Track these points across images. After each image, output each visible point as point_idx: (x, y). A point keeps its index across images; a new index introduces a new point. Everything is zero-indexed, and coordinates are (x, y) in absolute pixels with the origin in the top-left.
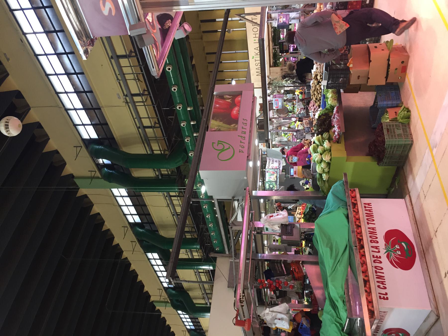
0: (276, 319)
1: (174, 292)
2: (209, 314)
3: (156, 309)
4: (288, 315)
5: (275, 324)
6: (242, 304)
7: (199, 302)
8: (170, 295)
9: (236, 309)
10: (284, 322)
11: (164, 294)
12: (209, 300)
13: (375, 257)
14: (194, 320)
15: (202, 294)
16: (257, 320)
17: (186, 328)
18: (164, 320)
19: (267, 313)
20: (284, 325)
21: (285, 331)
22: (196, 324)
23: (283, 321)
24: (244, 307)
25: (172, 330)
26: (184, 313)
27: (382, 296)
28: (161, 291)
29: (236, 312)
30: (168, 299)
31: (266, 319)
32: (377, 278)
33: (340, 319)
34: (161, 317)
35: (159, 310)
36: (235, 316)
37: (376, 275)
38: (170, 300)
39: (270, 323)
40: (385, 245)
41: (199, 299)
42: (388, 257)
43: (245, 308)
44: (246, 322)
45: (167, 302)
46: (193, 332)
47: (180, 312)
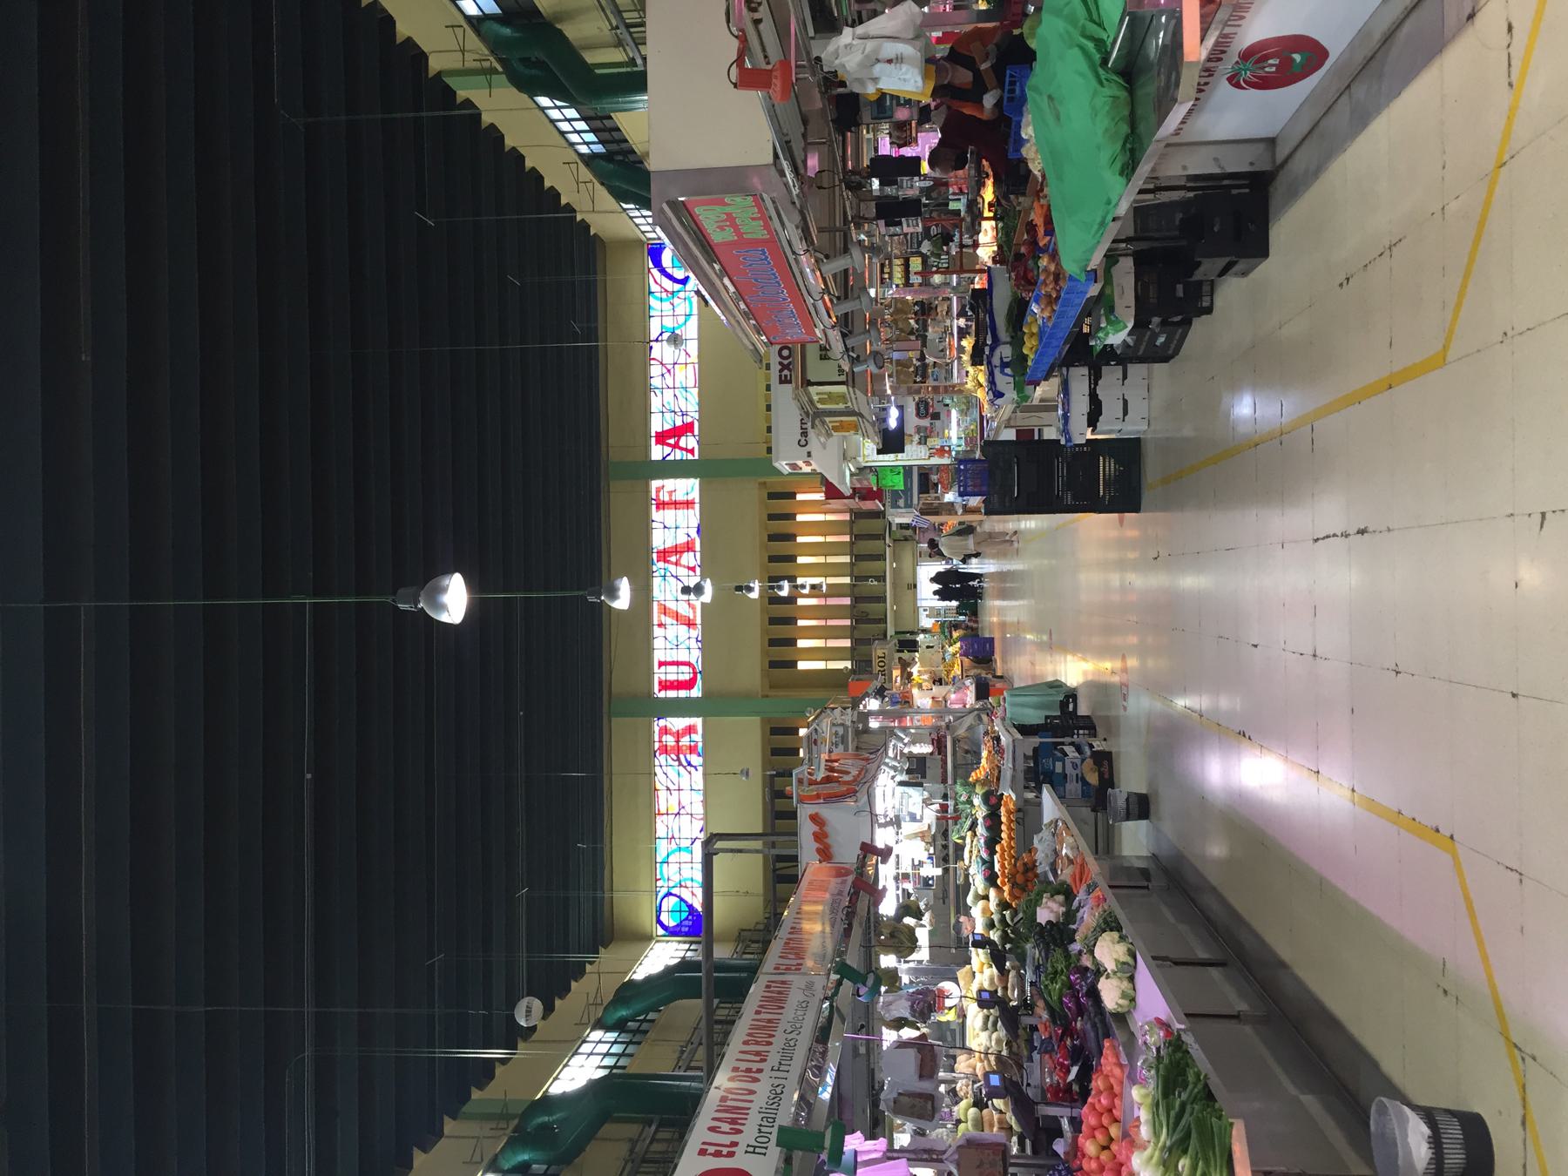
0: (878, 61)
1: (507, 31)
2: (646, 98)
3: (459, 100)
4: (918, 43)
5: (875, 80)
6: (757, 16)
7: (604, 57)
8: (495, 45)
9: (734, 29)
10: (904, 67)
11: (473, 41)
12: (640, 47)
14: (599, 122)
15: (613, 29)
16: (813, 74)
17: (576, 151)
18: (495, 135)
19: (846, 46)
20: (905, 80)
21: (908, 102)
22: (606, 136)
23: (903, 65)
24: (761, 27)
25: (529, 164)
26: (559, 103)
28: (459, 31)
29: (735, 43)
30: (491, 58)
31: (844, 66)
33: (1100, 25)
34: (506, 150)
35: (468, 103)
36: (735, 58)
38: (500, 60)
39: (858, 80)
41: (603, 50)
43: (767, 27)
44: (774, 73)
45: (493, 71)
46: (603, 163)
47: (544, 101)
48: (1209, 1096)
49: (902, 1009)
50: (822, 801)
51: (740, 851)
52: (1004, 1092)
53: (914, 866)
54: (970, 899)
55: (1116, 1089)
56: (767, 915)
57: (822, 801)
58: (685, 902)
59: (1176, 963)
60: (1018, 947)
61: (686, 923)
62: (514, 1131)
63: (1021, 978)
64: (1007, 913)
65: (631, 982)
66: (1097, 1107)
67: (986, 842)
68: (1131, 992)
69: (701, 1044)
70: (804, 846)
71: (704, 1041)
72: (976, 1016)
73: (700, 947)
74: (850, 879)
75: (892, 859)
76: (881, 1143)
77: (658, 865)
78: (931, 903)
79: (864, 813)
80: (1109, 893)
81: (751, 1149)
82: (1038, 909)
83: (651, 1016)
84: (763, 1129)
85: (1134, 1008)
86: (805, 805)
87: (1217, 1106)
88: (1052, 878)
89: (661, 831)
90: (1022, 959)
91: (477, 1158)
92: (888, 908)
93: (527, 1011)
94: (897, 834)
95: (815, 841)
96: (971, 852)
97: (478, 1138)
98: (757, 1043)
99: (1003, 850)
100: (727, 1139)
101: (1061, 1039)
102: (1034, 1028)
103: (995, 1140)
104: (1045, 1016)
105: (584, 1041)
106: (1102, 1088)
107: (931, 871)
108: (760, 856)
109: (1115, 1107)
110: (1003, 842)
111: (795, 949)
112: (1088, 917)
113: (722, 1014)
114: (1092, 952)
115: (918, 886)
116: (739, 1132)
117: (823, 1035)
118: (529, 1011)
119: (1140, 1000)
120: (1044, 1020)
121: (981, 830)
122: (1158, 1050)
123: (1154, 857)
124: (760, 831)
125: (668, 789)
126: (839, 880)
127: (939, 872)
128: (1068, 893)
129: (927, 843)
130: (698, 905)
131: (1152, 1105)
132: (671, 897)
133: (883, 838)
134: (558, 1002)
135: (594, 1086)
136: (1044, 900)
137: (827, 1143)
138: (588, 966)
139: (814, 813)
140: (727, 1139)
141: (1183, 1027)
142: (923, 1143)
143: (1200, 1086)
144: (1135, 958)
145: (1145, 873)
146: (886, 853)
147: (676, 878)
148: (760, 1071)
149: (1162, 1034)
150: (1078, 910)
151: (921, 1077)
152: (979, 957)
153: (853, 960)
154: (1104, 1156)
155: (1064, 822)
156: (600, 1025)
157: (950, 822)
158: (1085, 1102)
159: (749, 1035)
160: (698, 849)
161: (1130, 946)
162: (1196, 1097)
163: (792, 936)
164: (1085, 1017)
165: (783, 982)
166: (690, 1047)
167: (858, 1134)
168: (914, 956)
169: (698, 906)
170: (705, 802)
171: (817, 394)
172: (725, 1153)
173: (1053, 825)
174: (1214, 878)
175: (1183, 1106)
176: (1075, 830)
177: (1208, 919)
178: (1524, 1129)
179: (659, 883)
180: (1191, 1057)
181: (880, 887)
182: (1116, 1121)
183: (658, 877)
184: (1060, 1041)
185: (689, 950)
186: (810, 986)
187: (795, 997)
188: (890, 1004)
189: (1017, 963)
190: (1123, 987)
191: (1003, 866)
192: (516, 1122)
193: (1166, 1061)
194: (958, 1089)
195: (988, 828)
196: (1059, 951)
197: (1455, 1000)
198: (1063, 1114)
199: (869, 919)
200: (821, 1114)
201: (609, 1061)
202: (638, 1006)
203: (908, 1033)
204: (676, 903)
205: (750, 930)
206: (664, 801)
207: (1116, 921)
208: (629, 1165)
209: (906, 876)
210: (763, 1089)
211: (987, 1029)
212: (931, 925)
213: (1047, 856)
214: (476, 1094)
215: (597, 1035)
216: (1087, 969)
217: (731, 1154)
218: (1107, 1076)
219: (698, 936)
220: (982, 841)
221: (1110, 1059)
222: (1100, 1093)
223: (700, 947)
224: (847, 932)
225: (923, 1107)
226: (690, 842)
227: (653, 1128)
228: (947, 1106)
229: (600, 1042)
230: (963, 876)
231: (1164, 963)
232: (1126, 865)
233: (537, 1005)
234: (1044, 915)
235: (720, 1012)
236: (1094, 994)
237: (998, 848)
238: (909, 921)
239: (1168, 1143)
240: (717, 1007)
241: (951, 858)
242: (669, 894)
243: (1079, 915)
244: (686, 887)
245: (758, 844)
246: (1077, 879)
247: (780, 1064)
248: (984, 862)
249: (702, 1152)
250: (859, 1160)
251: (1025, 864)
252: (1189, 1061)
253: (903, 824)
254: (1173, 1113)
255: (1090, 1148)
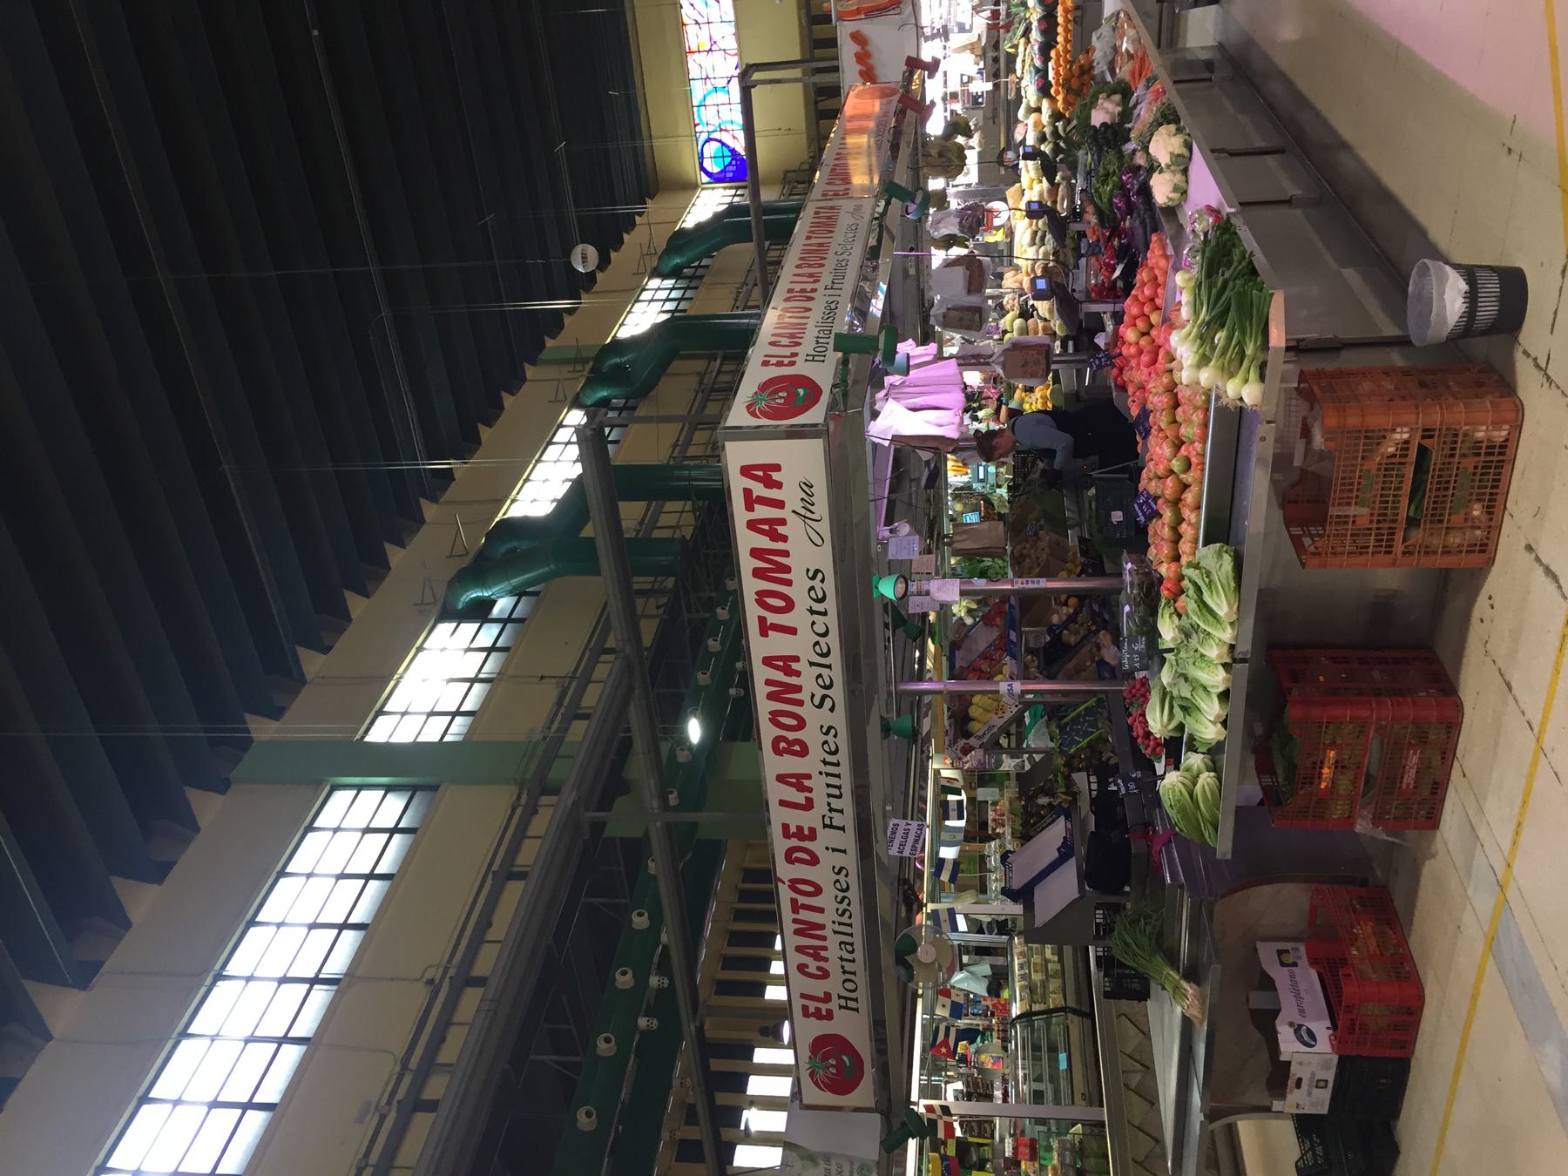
13: (794, 835)
27: (812, 1006)
32: (797, 932)
37: (795, 921)
40: (810, 1057)
42: (812, 1075)
48: (1253, 272)
49: (950, 227)
50: (863, 16)
51: (778, 81)
52: (1050, 293)
53: (963, 84)
54: (1021, 114)
55: (1160, 279)
56: (812, 154)
57: (863, 16)
58: (728, 147)
59: (1232, 155)
60: (1070, 156)
61: (731, 168)
62: (591, 371)
63: (1071, 188)
64: (1060, 124)
65: (682, 230)
66: (1140, 298)
67: (1040, 49)
68: (1184, 185)
69: (756, 285)
70: (846, 69)
71: (758, 282)
72: (1023, 233)
73: (746, 192)
74: (896, 98)
75: (939, 75)
76: (932, 348)
77: (695, 109)
78: (981, 124)
79: (910, 26)
80: (1170, 85)
81: (811, 358)
82: (1093, 112)
83: (705, 262)
84: (820, 340)
85: (1185, 200)
86: (846, 23)
87: (1259, 279)
88: (1109, 78)
89: (694, 72)
90: (1073, 167)
91: (561, 396)
92: (935, 126)
93: (583, 258)
94: (945, 48)
95: (858, 62)
96: (1024, 61)
97: (559, 380)
98: (810, 266)
99: (1058, 55)
100: (787, 351)
101: (1109, 239)
102: (1082, 235)
103: (1040, 342)
104: (1094, 220)
105: (644, 290)
106: (1146, 280)
107: (982, 86)
108: (800, 85)
109: (1157, 296)
110: (1059, 46)
111: (841, 175)
112: (1145, 112)
113: (773, 255)
114: (1146, 149)
115: (967, 105)
116: (798, 344)
117: (873, 253)
118: (584, 258)
119: (1192, 191)
120: (1092, 224)
121: (1035, 35)
122: (1206, 234)
123: (1221, 46)
124: (798, 57)
125: (697, 23)
126: (885, 100)
127: (989, 86)
128: (1125, 91)
129: (977, 56)
130: (740, 147)
131: (1194, 287)
132: (712, 142)
133: (928, 52)
134: (613, 255)
135: (658, 330)
136: (1100, 101)
137: (881, 345)
138: (637, 218)
139: (854, 31)
140: (787, 351)
141: (1233, 210)
142: (970, 350)
143: (1244, 264)
144: (1190, 149)
145: (1209, 65)
146: (933, 67)
147: (715, 121)
148: (814, 290)
149: (1211, 220)
150: (1135, 107)
151: (969, 292)
152: (1029, 170)
153: (902, 178)
154: (1143, 342)
155: (1127, 14)
156: (656, 273)
157: (1002, 31)
158: (1128, 295)
159: (801, 259)
160: (735, 87)
161: (1187, 137)
162: (1239, 274)
163: (837, 162)
164: (1135, 215)
165: (832, 208)
166: (745, 287)
167: (910, 341)
168: (960, 179)
169: (740, 149)
170: (738, 35)
171: (792, 631)
172: (786, 363)
173: (1114, 19)
174: (1283, 61)
175: (1225, 284)
176: (1137, 21)
177: (1272, 108)
178: (1563, 277)
179: (698, 129)
180: (1239, 238)
181: (928, 102)
182: (1158, 308)
183: (697, 122)
184: (1108, 242)
185: (735, 195)
186: (858, 208)
187: (845, 220)
188: (939, 222)
189: (1069, 173)
190: (1175, 181)
191: (1057, 73)
192: (591, 364)
193: (1213, 243)
194: (1004, 303)
195: (1043, 32)
196: (1112, 152)
197: (1518, 158)
198: (1105, 309)
199: (916, 140)
200: (873, 328)
201: (670, 306)
202: (690, 254)
203: (956, 251)
204: (718, 149)
205: (794, 171)
206: (694, 37)
207: (1175, 113)
208: (700, 394)
209: (954, 96)
210: (818, 308)
211: (1035, 244)
212: (980, 146)
213: (1105, 54)
214: (550, 343)
215: (655, 283)
216: (1140, 167)
217: (792, 364)
218: (1152, 268)
219: (744, 180)
220: (1036, 47)
221: (1156, 252)
222: (1144, 284)
223: (746, 192)
224: (895, 148)
225: (970, 318)
226: (726, 81)
227: (718, 362)
228: (994, 320)
229: (659, 289)
230: (1014, 91)
231: (1221, 155)
232: (1189, 57)
233: (592, 251)
234: (1098, 118)
235: (772, 253)
236: (1146, 191)
237: (1053, 54)
238: (960, 140)
239: (1207, 319)
240: (769, 249)
241: (1002, 73)
242: (709, 140)
243: (1136, 112)
244: (726, 130)
245: (796, 73)
246: (1137, 73)
247: (833, 283)
248: (1038, 71)
249: (765, 364)
250: (911, 363)
251: (1081, 67)
252: (1236, 241)
253: (951, 36)
254: (1214, 291)
255: (1130, 335)
